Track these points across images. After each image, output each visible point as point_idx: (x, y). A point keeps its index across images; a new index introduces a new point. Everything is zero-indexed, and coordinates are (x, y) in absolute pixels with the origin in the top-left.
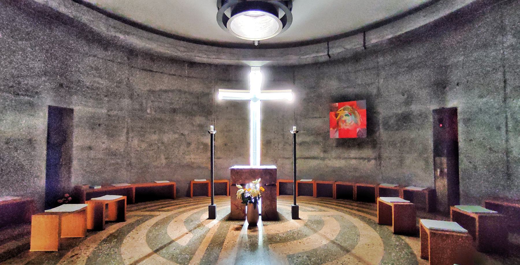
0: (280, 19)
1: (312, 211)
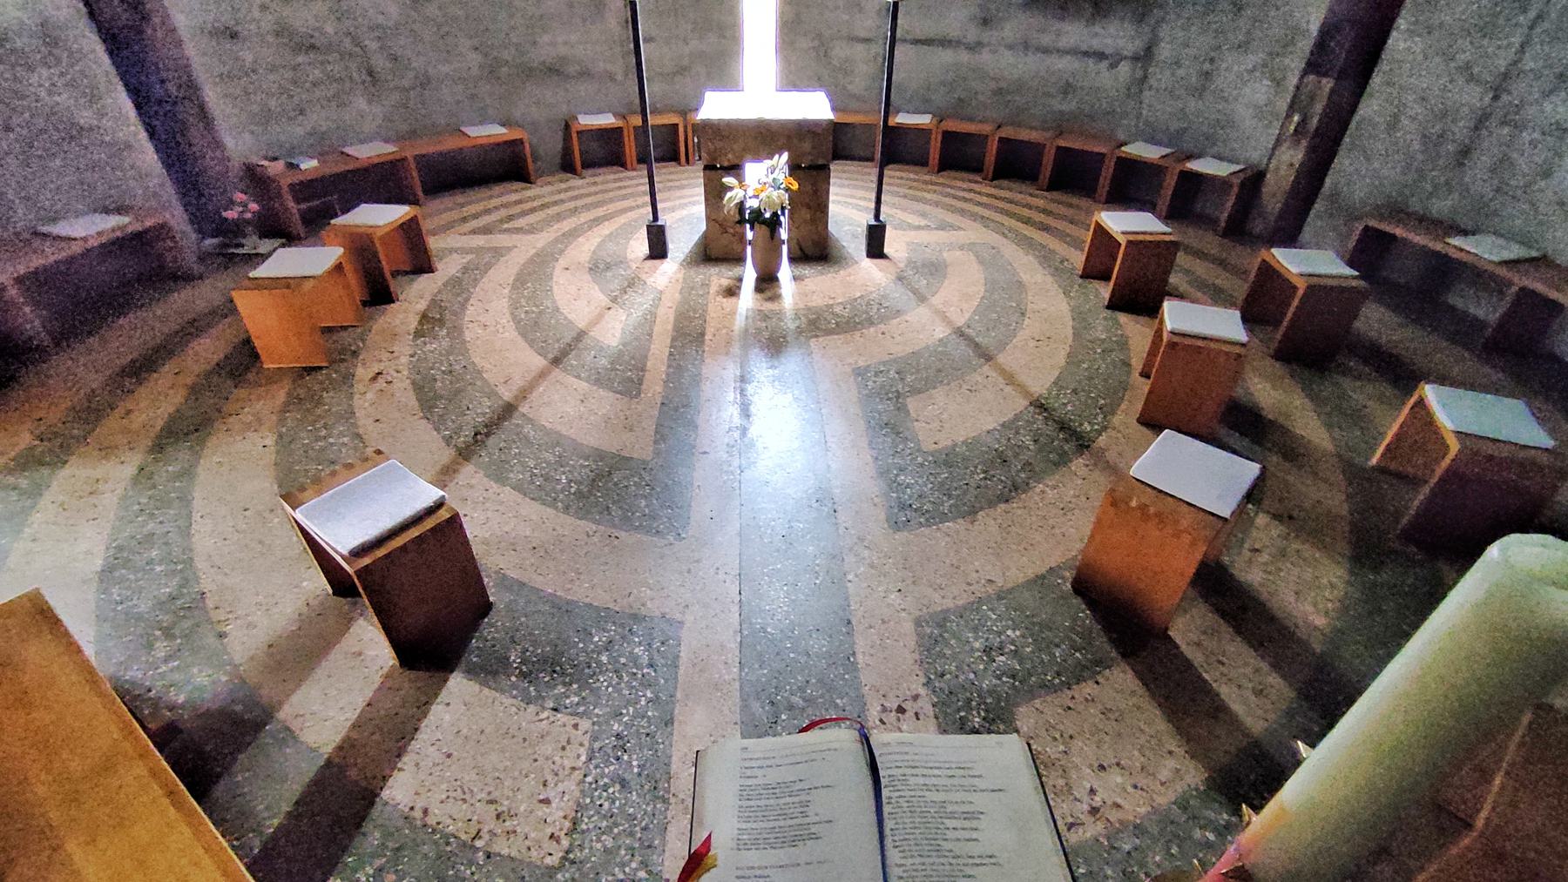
1: (919, 228)
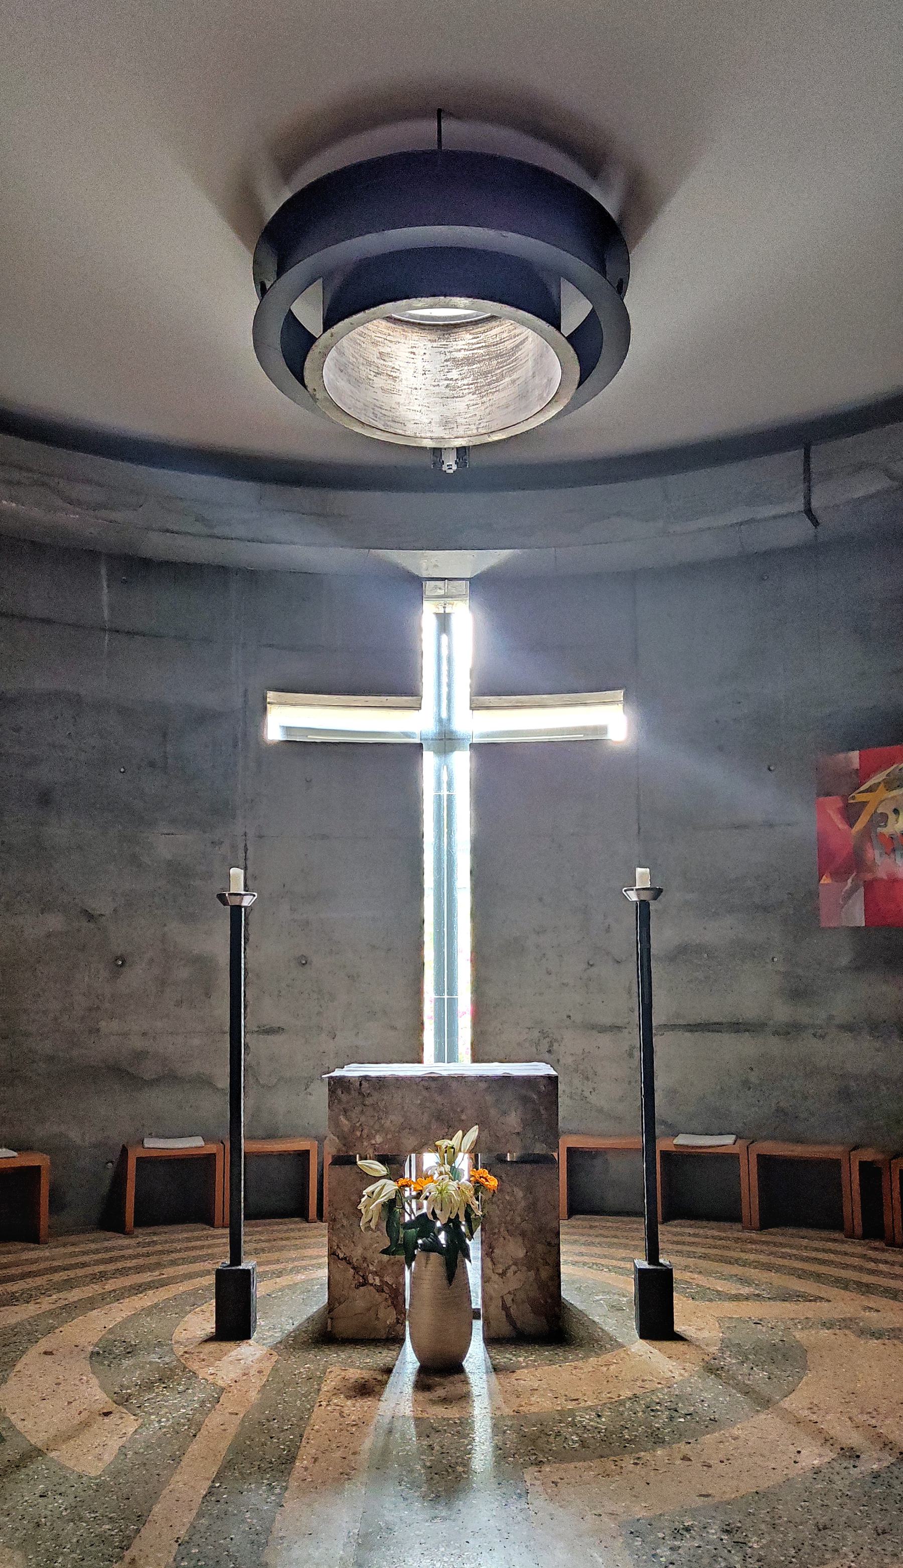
0: (569, 339)
1: (737, 1298)
